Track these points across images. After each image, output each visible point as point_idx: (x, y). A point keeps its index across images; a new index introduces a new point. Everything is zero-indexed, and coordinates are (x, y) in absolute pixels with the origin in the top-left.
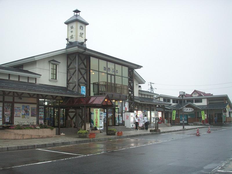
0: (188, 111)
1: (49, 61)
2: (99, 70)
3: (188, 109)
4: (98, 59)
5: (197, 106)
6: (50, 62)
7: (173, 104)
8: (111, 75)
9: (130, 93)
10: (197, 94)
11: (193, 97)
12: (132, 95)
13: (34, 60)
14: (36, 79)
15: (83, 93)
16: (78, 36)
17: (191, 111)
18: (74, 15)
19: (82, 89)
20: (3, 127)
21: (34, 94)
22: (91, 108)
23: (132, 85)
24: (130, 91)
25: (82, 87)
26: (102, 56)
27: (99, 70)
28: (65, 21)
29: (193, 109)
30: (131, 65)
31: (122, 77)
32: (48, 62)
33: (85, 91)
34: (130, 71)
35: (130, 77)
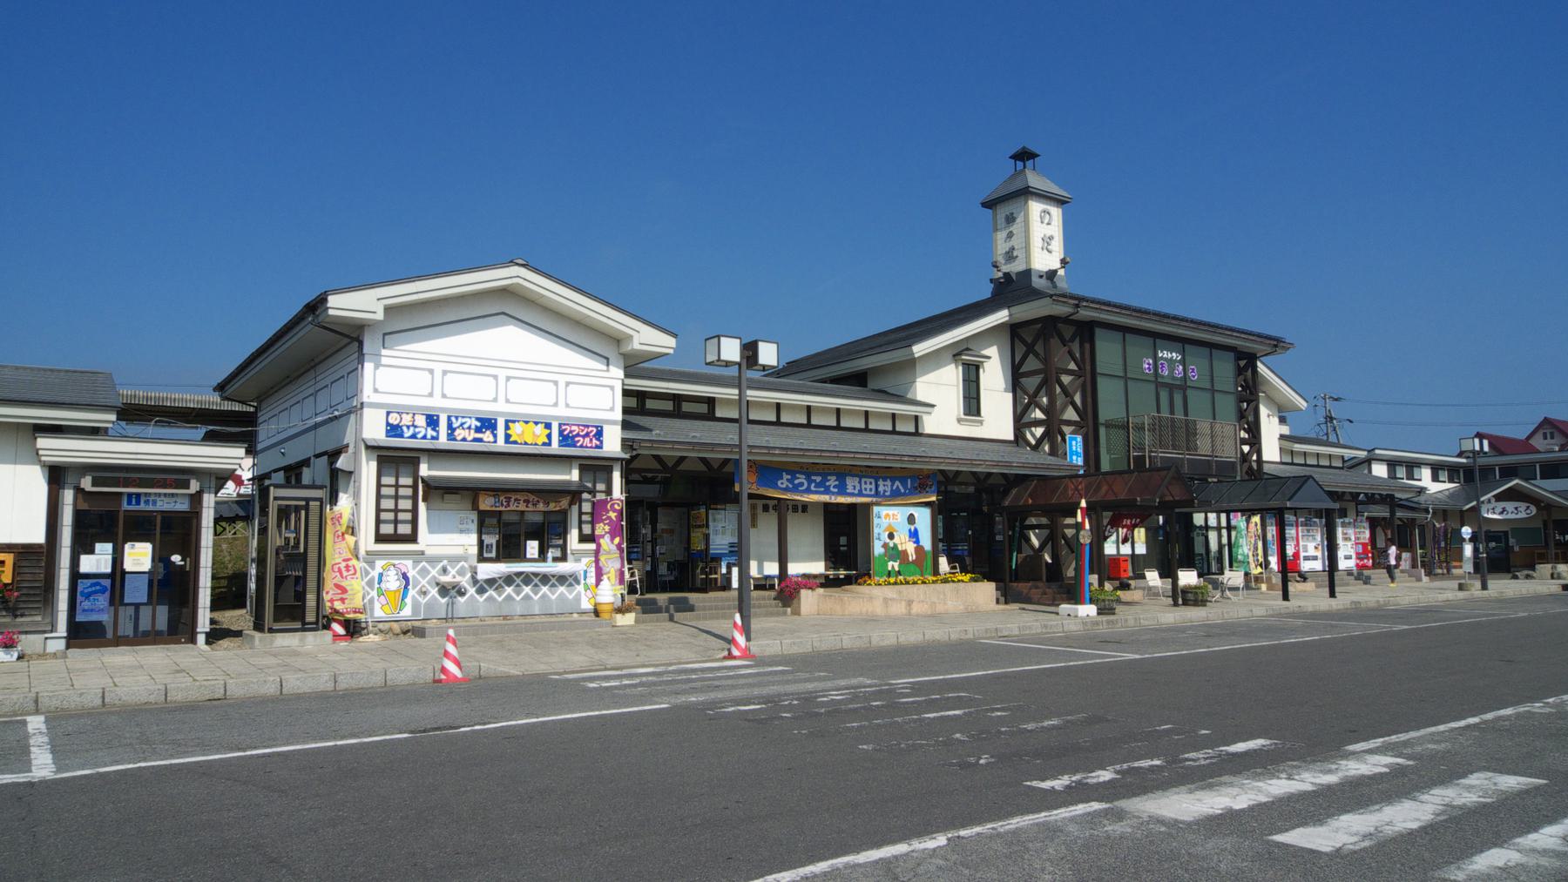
0: (1510, 516)
1: (954, 356)
2: (1125, 370)
3: (1510, 506)
4: (1181, 344)
5: (1552, 492)
6: (957, 358)
7: (1434, 488)
8: (1171, 388)
9: (1246, 448)
10: (1556, 434)
11: (1538, 452)
12: (1255, 458)
13: (909, 358)
14: (916, 418)
15: (1074, 458)
16: (1036, 250)
17: (1520, 516)
18: (1523, 436)
19: (1071, 446)
20: (827, 577)
21: (957, 471)
22: (765, 563)
23: (1251, 418)
24: (1244, 442)
25: (1071, 439)
26: (1209, 337)
27: (1125, 370)
28: (982, 198)
29: (1534, 510)
30: (1255, 346)
31: (1126, 378)
32: (951, 356)
33: (1080, 450)
34: (1242, 363)
35: (1242, 386)
